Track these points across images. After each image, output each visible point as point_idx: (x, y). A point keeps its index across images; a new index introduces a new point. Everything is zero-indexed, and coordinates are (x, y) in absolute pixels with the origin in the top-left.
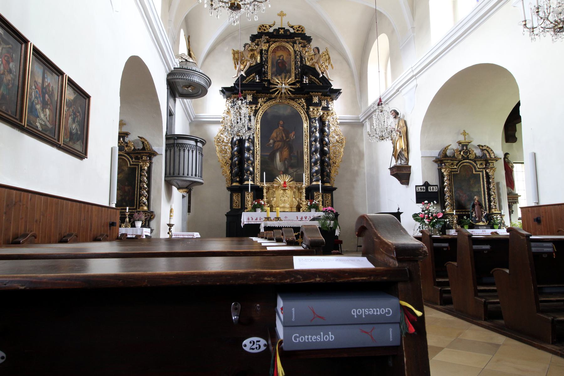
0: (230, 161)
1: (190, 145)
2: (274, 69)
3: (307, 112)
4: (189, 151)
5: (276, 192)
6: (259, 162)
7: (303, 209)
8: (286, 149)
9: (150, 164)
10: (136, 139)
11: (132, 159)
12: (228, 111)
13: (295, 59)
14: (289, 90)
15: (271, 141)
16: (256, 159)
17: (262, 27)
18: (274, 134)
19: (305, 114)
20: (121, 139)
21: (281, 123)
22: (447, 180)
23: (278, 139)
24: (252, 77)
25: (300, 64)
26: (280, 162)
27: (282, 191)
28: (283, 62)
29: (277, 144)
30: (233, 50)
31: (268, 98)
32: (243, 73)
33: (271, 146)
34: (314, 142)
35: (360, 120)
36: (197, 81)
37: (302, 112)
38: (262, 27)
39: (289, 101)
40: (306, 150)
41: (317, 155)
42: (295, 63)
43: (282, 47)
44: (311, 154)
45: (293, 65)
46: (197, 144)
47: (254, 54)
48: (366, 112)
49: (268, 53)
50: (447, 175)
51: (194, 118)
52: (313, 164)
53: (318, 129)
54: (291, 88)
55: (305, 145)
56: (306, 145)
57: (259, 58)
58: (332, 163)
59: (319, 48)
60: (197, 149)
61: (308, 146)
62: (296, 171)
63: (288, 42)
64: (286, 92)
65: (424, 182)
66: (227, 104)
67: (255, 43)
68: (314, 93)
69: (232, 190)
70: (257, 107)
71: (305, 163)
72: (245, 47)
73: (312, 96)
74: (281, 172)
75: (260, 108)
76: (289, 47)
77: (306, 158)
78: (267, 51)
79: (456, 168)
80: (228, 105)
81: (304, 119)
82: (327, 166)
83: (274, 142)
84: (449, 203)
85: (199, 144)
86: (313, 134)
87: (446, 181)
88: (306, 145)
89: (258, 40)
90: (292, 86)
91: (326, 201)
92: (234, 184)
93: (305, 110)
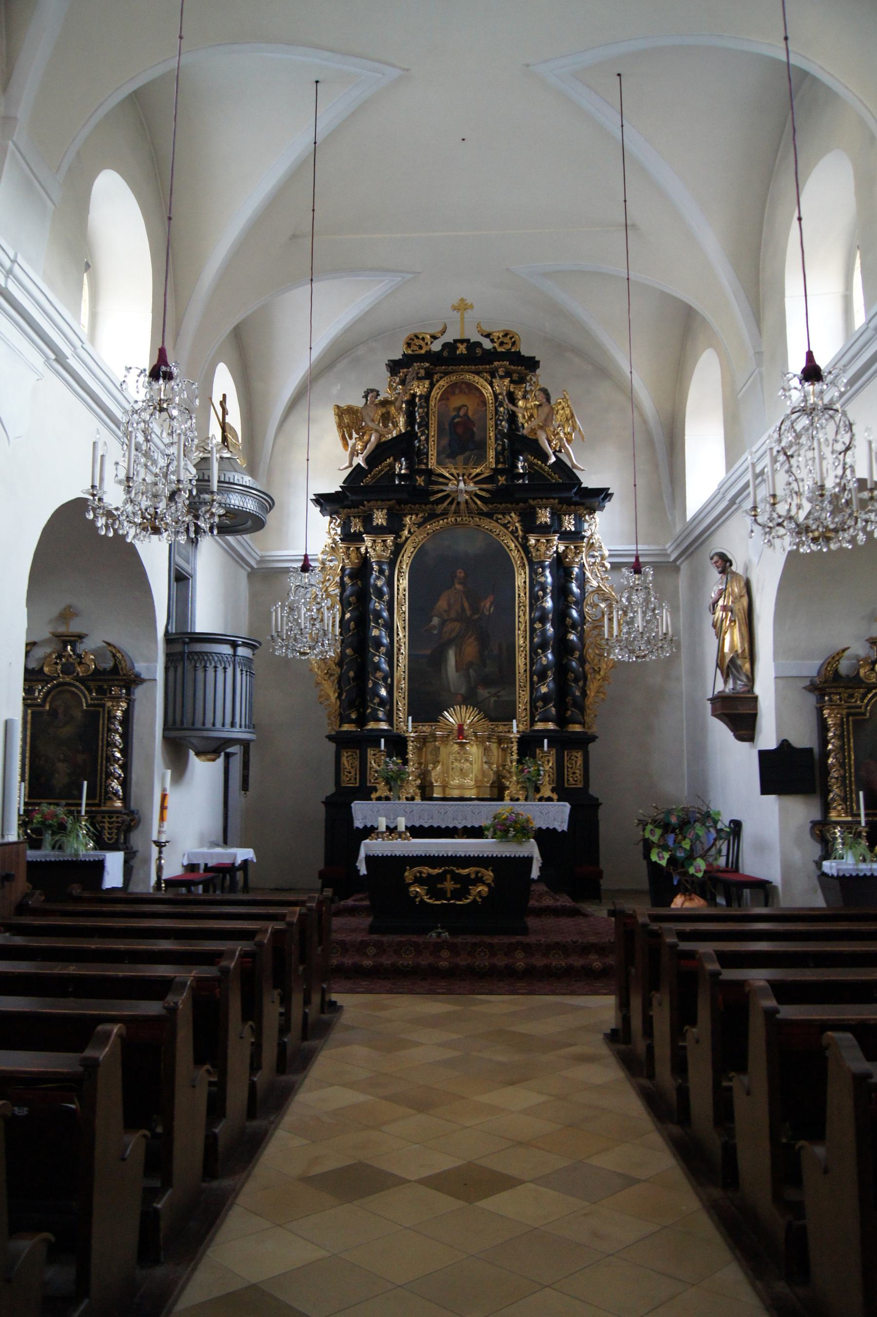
0: (338, 670)
1: (220, 654)
2: (445, 442)
3: (525, 547)
4: (218, 669)
5: (443, 750)
6: (404, 672)
7: (510, 793)
8: (472, 640)
9: (128, 704)
10: (99, 645)
11: (90, 692)
12: (334, 546)
13: (496, 415)
14: (477, 495)
15: (436, 621)
16: (398, 665)
17: (413, 340)
18: (442, 604)
19: (518, 551)
20: (69, 647)
21: (460, 573)
22: (833, 738)
23: (453, 615)
24: (386, 467)
25: (507, 425)
26: (457, 672)
27: (456, 747)
28: (467, 423)
29: (450, 626)
30: (338, 407)
31: (429, 514)
32: (359, 460)
33: (436, 632)
34: (540, 622)
35: (668, 556)
36: (237, 503)
37: (513, 545)
38: (413, 340)
39: (480, 519)
40: (521, 642)
41: (546, 656)
42: (496, 425)
43: (464, 386)
44: (535, 651)
45: (491, 429)
46: (235, 651)
47: (388, 413)
48: (680, 540)
49: (431, 402)
50: (835, 724)
51: (258, 562)
52: (535, 678)
53: (548, 591)
54: (480, 489)
55: (519, 629)
56: (522, 629)
57: (402, 420)
58: (591, 671)
59: (550, 391)
60: (236, 662)
61: (526, 631)
62: (495, 695)
63: (478, 373)
64: (470, 501)
65: (780, 742)
66: (331, 530)
67: (400, 377)
68: (539, 500)
69: (341, 741)
70: (401, 537)
71: (519, 673)
72: (366, 397)
73: (535, 509)
74: (460, 698)
75: (407, 539)
76: (481, 382)
77: (521, 662)
78: (426, 398)
79: (860, 707)
80: (333, 532)
81: (516, 563)
82: (576, 680)
83: (443, 623)
84: (838, 796)
85: (241, 651)
86: (536, 602)
87: (833, 741)
88: (522, 629)
89: (405, 370)
90: (484, 486)
91: (570, 770)
92: (346, 727)
93: (520, 539)
